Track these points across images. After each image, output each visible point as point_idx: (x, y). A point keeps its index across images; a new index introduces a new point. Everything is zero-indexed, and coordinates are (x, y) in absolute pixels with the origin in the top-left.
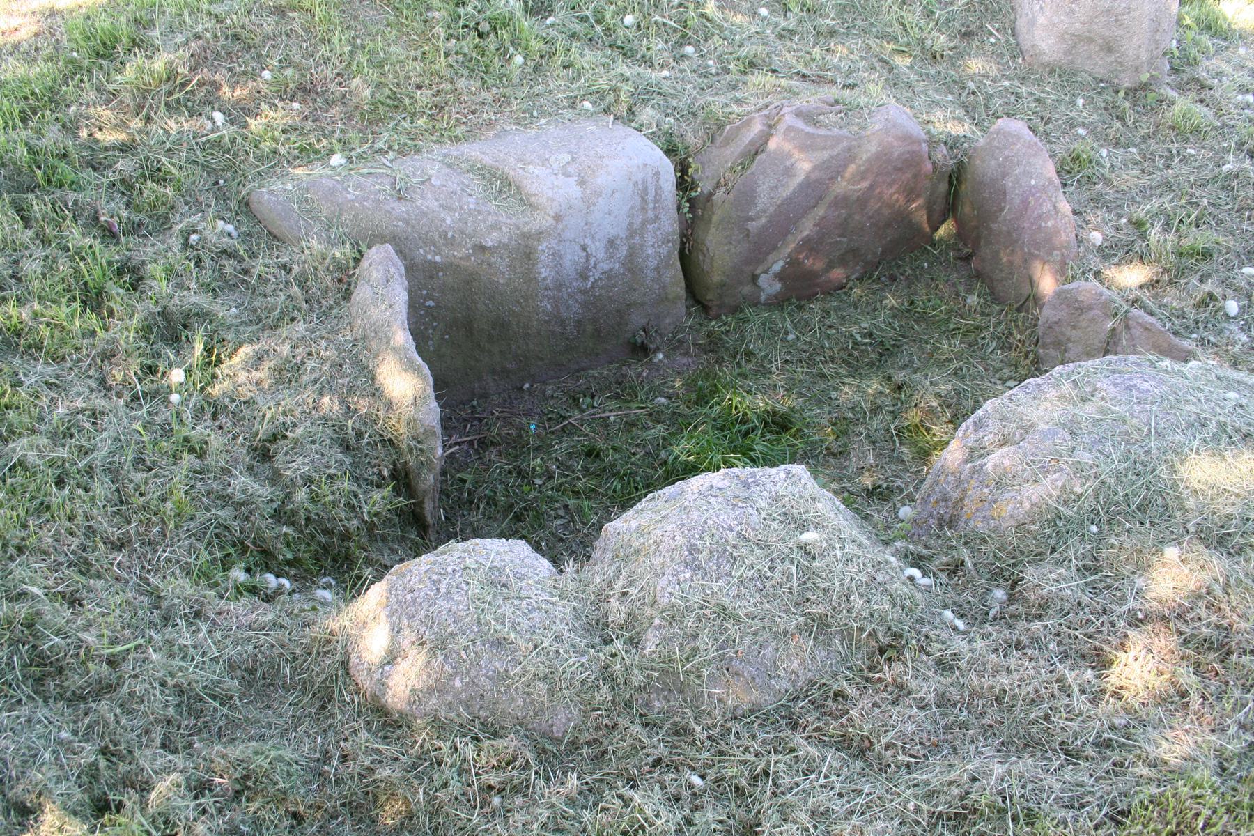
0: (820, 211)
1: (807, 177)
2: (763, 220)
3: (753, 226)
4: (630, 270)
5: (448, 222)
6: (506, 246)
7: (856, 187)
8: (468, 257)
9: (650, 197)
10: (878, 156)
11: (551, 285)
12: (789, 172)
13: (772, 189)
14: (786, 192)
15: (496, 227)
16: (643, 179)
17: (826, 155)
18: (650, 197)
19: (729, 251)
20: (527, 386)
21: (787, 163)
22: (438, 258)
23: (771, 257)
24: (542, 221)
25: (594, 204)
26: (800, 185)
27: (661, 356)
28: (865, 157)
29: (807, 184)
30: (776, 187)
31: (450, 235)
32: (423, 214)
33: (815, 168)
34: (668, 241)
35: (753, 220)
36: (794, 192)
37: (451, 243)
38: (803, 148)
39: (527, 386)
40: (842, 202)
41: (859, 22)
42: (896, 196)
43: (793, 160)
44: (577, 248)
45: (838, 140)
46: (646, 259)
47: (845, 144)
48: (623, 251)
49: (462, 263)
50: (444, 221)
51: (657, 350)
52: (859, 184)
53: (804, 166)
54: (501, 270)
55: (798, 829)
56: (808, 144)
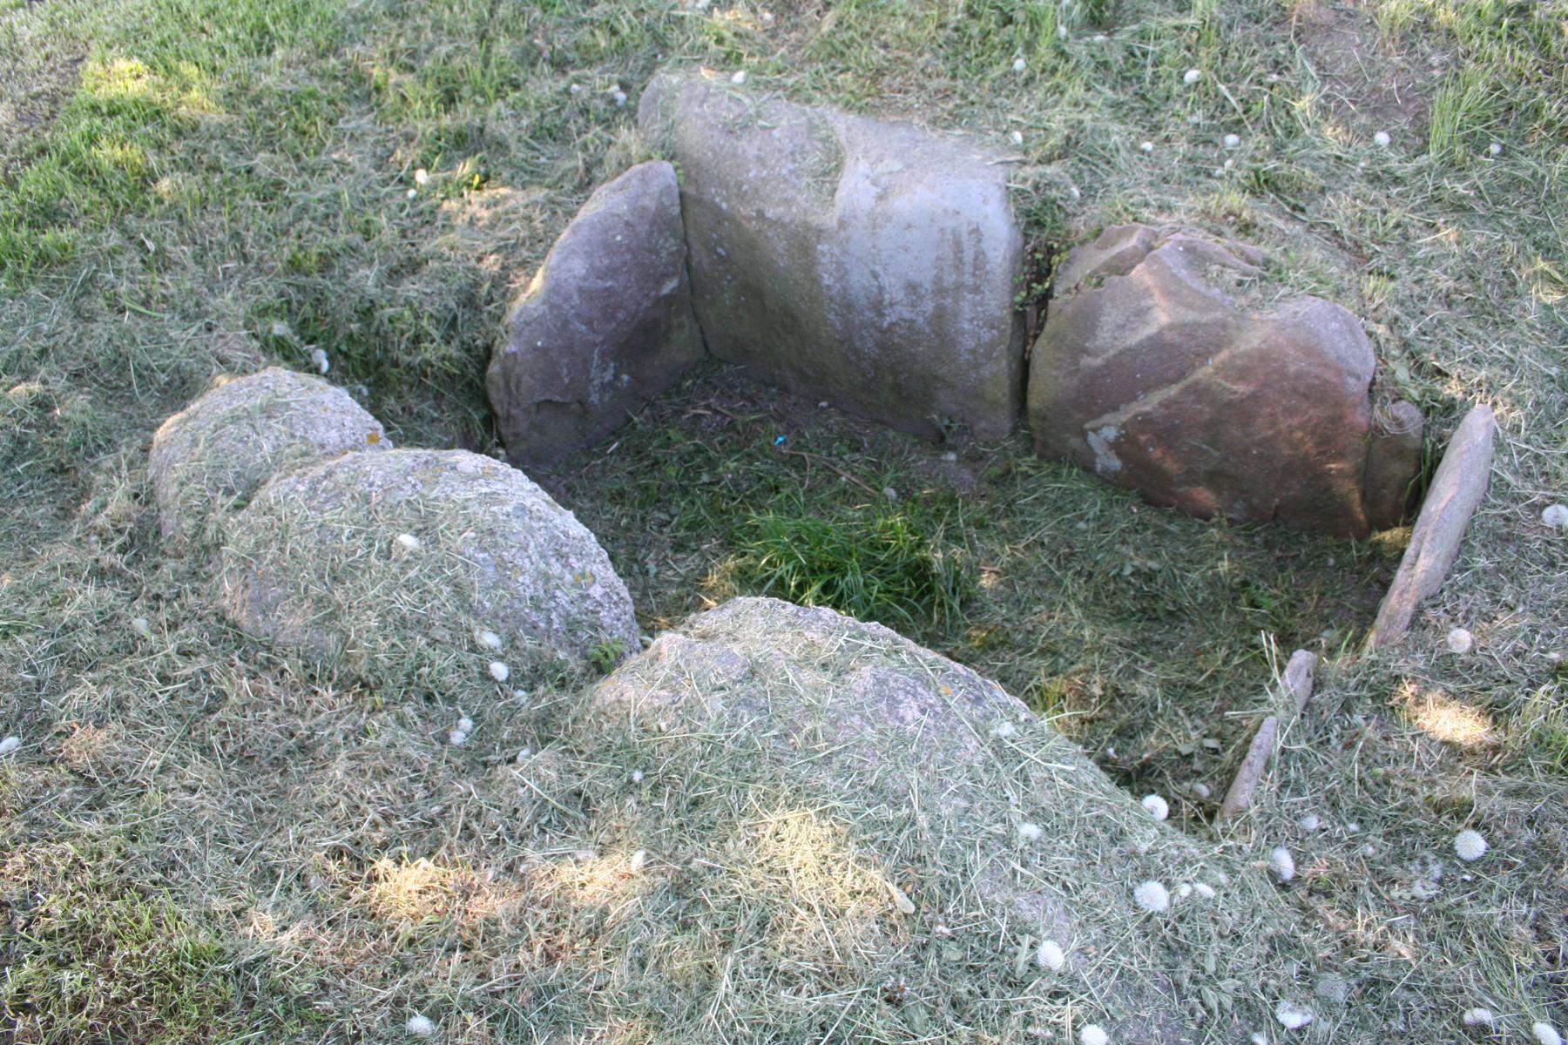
0: (1173, 391)
1: (1160, 333)
2: (1099, 362)
3: (1088, 362)
4: (938, 335)
5: (751, 175)
6: (784, 225)
7: (1228, 385)
8: (750, 219)
9: (968, 256)
10: (1263, 357)
11: (838, 300)
12: (1142, 314)
13: (1118, 327)
14: (1133, 340)
15: (788, 202)
16: (954, 230)
17: (1190, 316)
18: (968, 256)
19: (1056, 378)
20: (824, 404)
21: (1144, 303)
22: (724, 205)
23: (1107, 418)
24: (829, 220)
25: (882, 227)
26: (1150, 338)
27: (952, 457)
28: (1243, 348)
29: (1155, 343)
30: (1124, 326)
31: (745, 187)
32: (735, 155)
33: (1171, 327)
34: (992, 327)
35: (1089, 354)
36: (1140, 343)
37: (742, 196)
38: (1168, 294)
39: (824, 404)
40: (1199, 392)
41: (1524, 213)
42: (1299, 434)
43: (1151, 302)
44: (866, 271)
45: (1210, 305)
46: (962, 332)
47: (1219, 314)
48: (929, 306)
49: (744, 222)
50: (748, 171)
51: (953, 448)
52: (1234, 383)
53: (1162, 316)
54: (778, 248)
55: (195, 591)
56: (1174, 291)
